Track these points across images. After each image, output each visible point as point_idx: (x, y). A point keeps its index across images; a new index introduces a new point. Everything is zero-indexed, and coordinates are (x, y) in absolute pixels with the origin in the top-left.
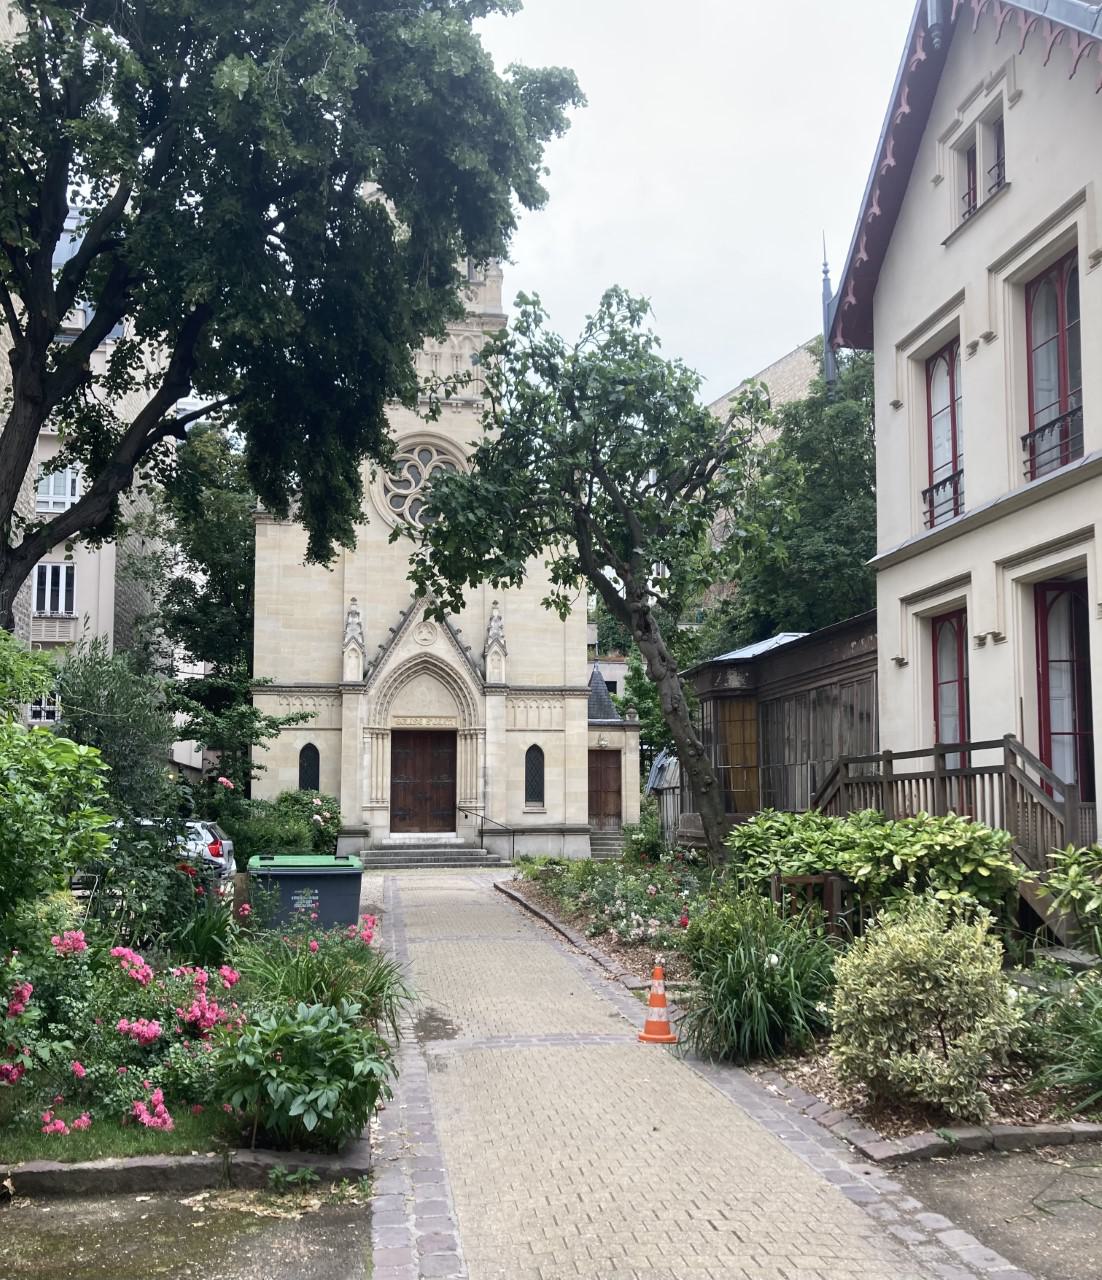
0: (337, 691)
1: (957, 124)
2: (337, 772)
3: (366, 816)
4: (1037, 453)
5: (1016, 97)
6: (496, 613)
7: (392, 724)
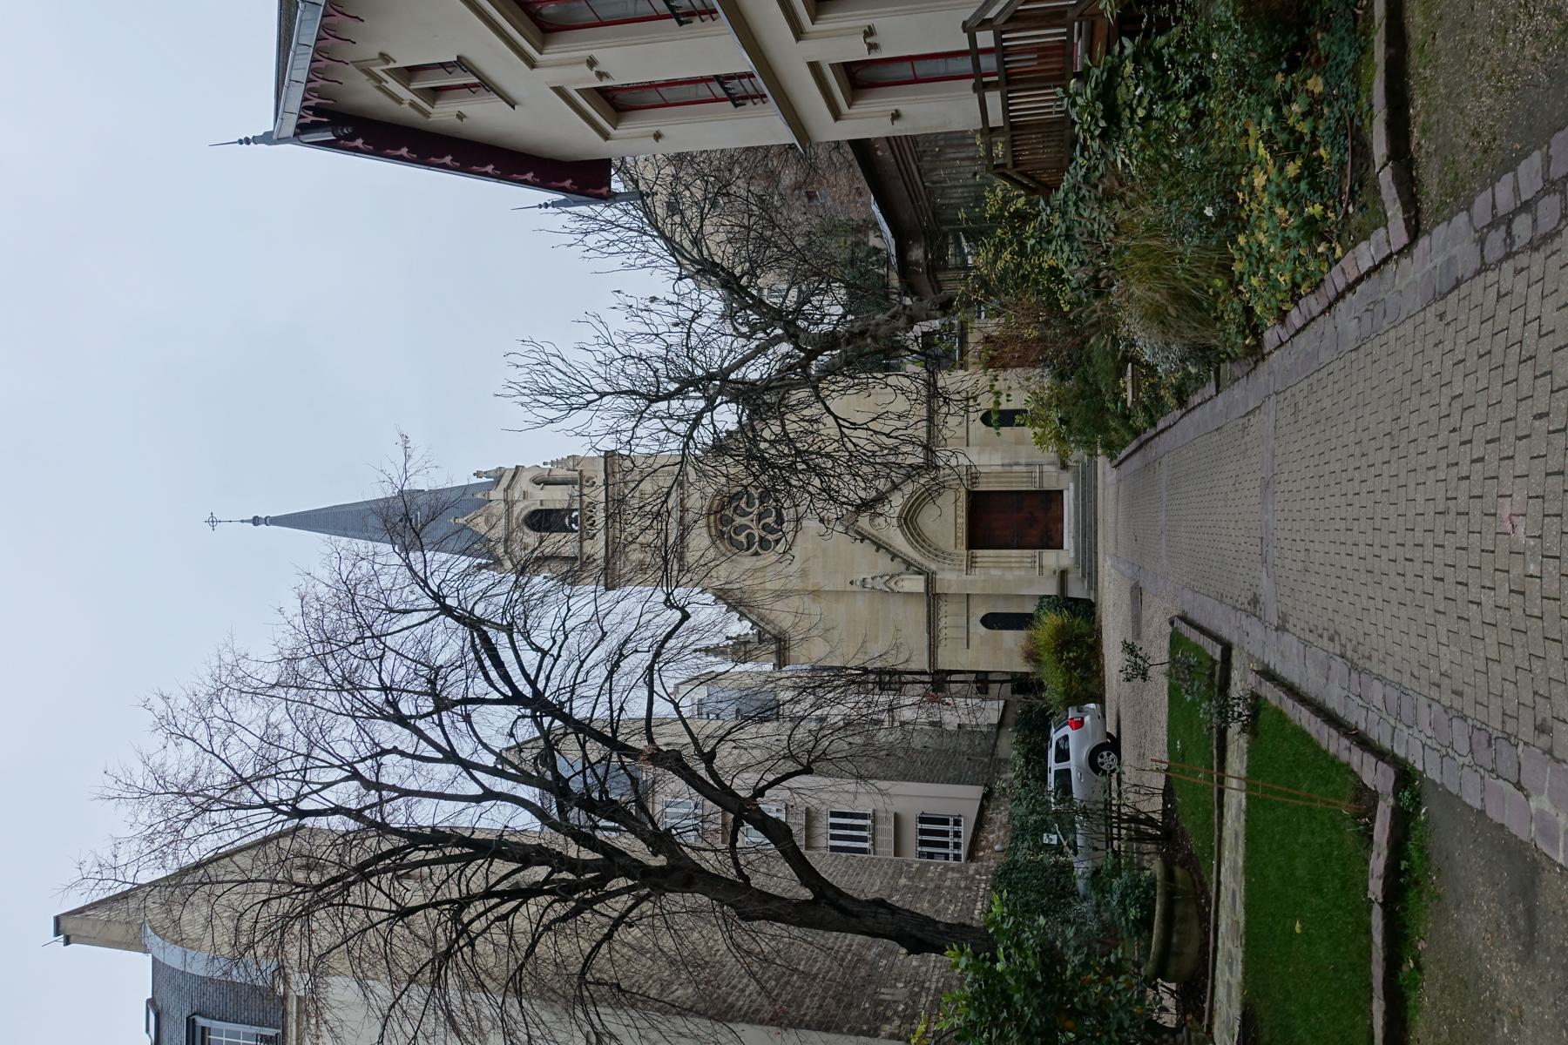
0: (932, 597)
1: (413, 104)
5: (384, 57)
7: (963, 550)
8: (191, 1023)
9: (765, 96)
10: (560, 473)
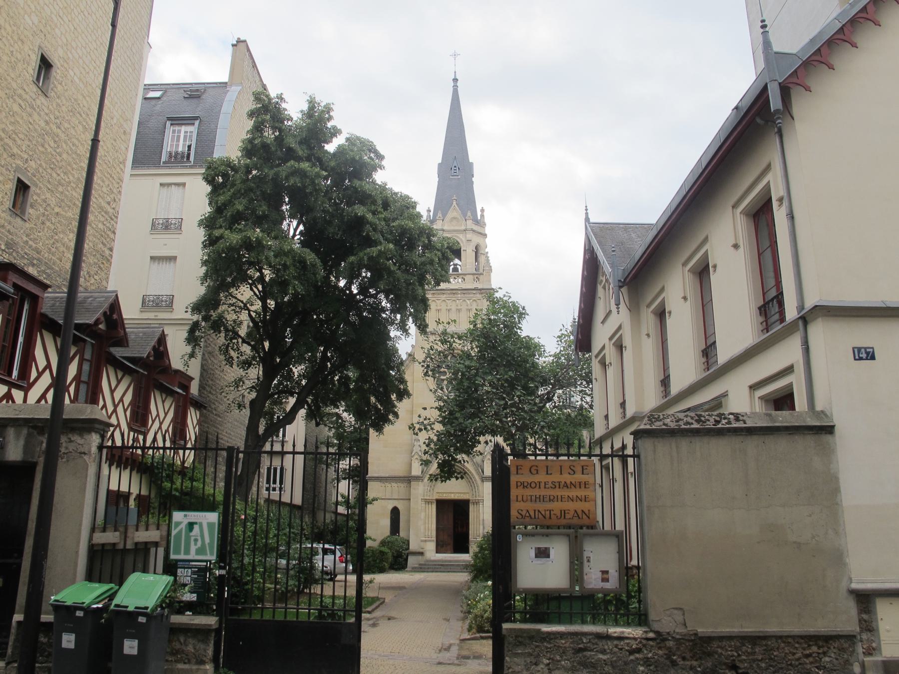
0: (408, 480)
2: (408, 521)
4: (768, 317)
7: (436, 497)
8: (196, 118)
9: (708, 370)
10: (482, 259)
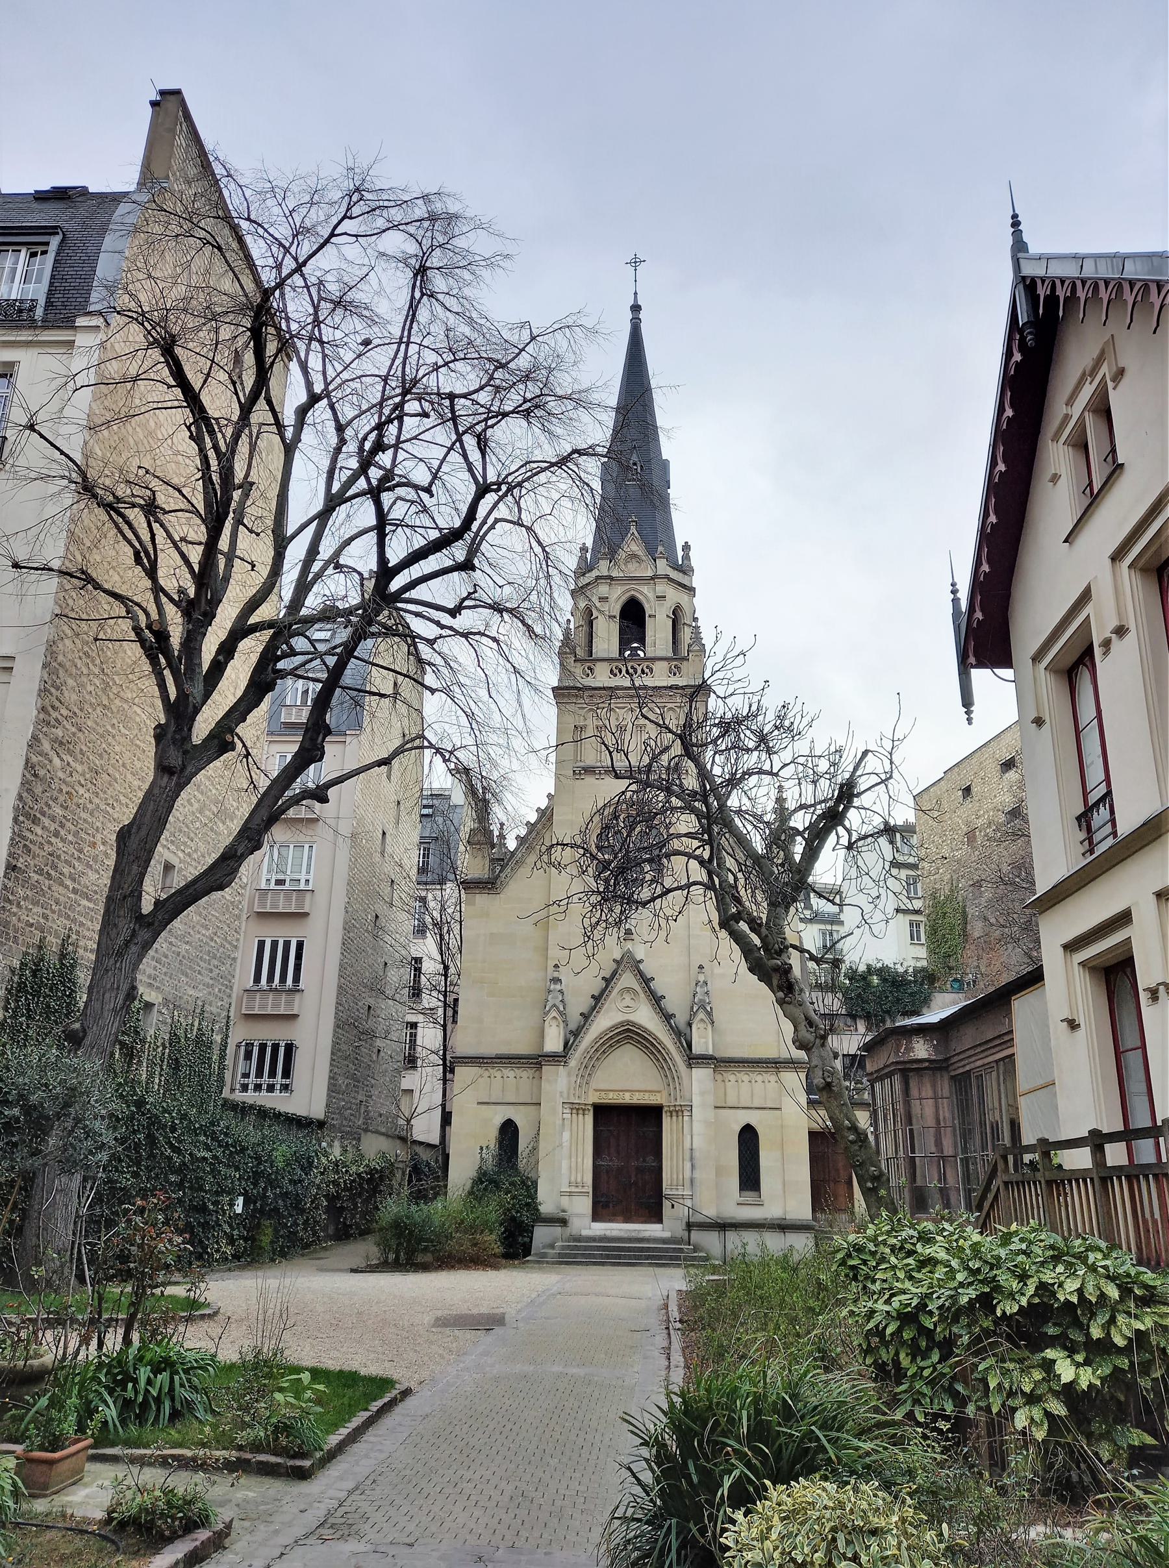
0: (537, 1061)
1: (1067, 418)
3: (565, 1202)
5: (1120, 374)
6: (701, 978)
7: (594, 1098)
8: (52, 231)
10: (686, 635)
